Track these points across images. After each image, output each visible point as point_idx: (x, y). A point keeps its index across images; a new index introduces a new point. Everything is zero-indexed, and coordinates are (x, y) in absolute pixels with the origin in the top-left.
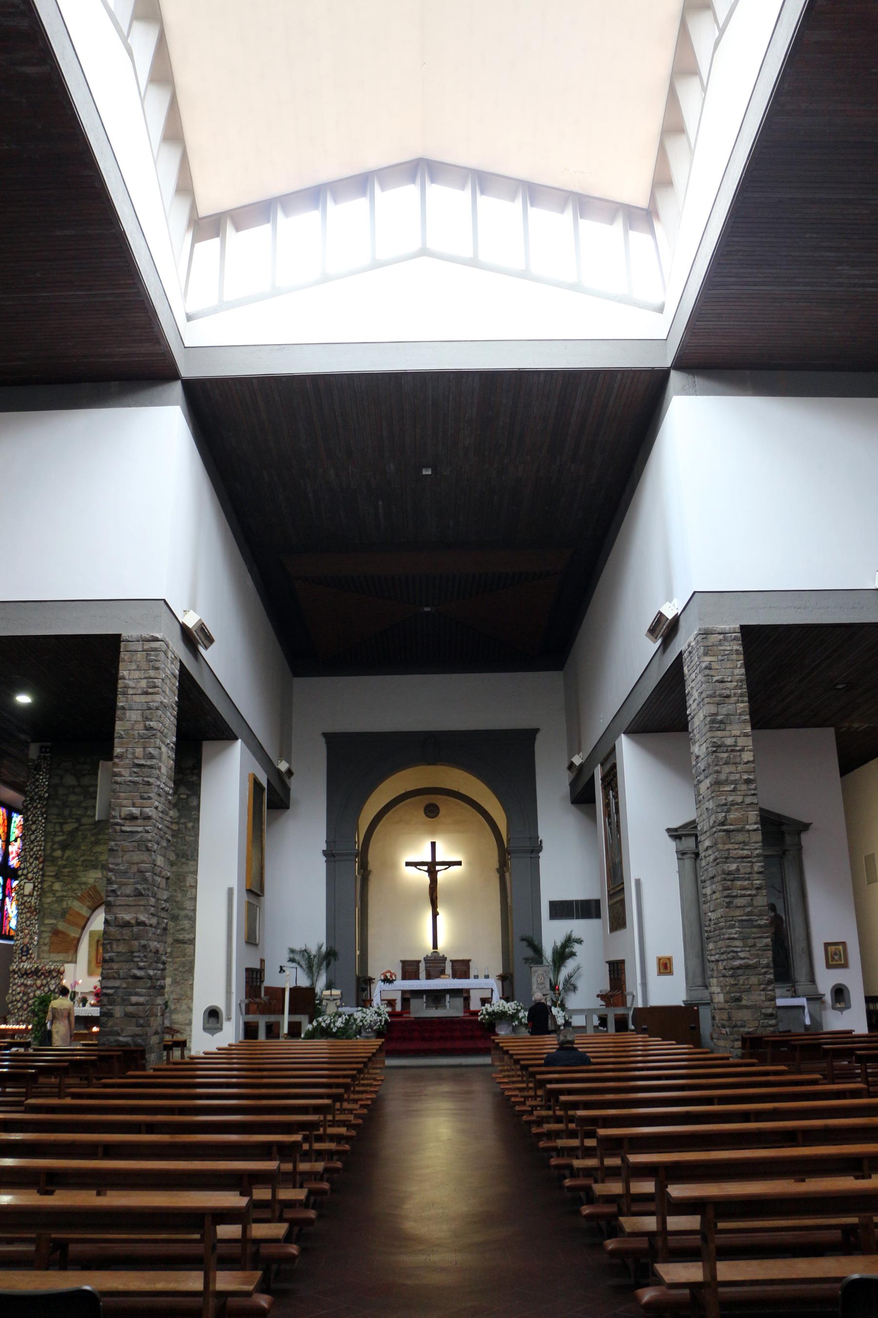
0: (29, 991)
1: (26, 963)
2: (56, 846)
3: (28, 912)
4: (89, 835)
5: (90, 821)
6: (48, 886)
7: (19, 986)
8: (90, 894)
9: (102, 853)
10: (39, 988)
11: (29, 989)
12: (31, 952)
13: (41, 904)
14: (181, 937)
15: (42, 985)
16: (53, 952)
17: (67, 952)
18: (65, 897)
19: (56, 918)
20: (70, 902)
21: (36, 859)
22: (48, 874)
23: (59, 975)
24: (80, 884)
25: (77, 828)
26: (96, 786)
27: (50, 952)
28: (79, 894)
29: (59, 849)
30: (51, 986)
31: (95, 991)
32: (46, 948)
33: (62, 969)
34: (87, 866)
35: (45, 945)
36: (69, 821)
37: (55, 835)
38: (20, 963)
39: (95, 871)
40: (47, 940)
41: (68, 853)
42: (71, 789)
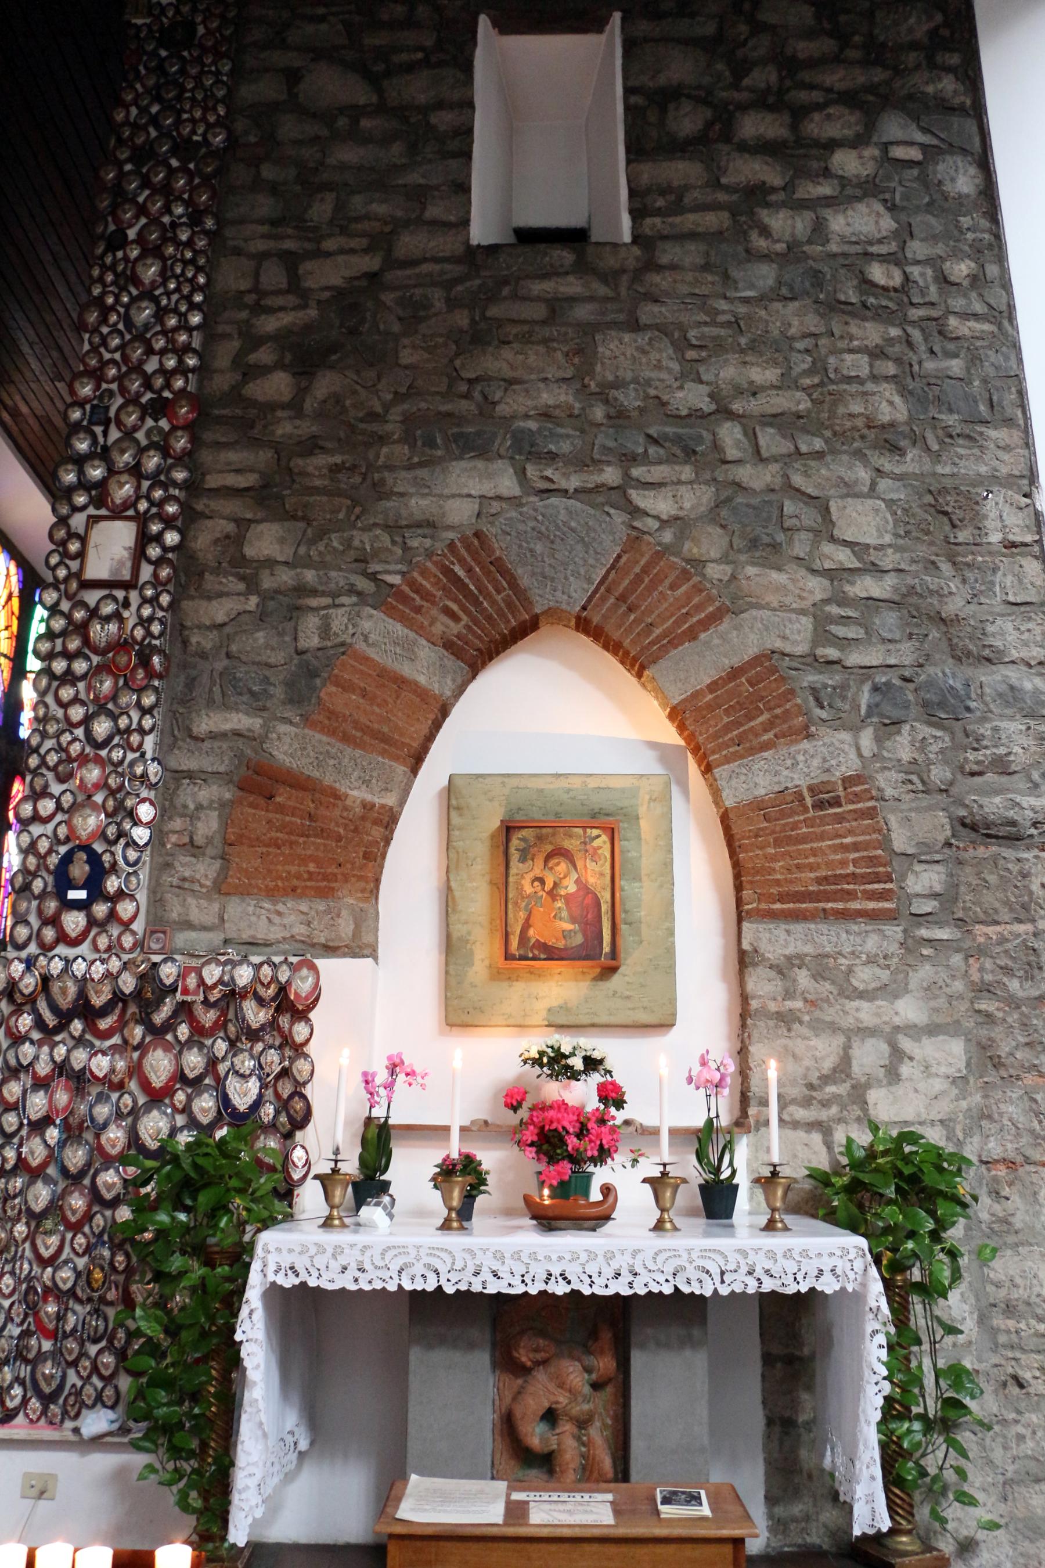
0: (102, 1111)
1: (85, 948)
2: (264, 355)
3: (99, 669)
4: (439, 305)
5: (445, 244)
6: (216, 541)
7: (41, 1084)
8: (456, 580)
9: (510, 382)
10: (157, 1097)
11: (101, 1098)
12: (112, 884)
13: (178, 631)
14: (994, 806)
15: (180, 1077)
16: (243, 892)
17: (325, 893)
18: (314, 592)
19: (257, 702)
20: (339, 619)
21: (159, 408)
22: (213, 481)
23: (284, 1021)
24: (393, 528)
25: (373, 277)
26: (469, 105)
27: (221, 888)
28: (396, 579)
29: (280, 365)
30: (233, 1085)
31: (513, 1119)
32: (205, 870)
33: (302, 986)
34: (431, 443)
35: (193, 848)
36: (329, 245)
37: (259, 309)
38: (46, 948)
39: (480, 464)
40: (208, 826)
41: (325, 384)
42: (342, 122)
